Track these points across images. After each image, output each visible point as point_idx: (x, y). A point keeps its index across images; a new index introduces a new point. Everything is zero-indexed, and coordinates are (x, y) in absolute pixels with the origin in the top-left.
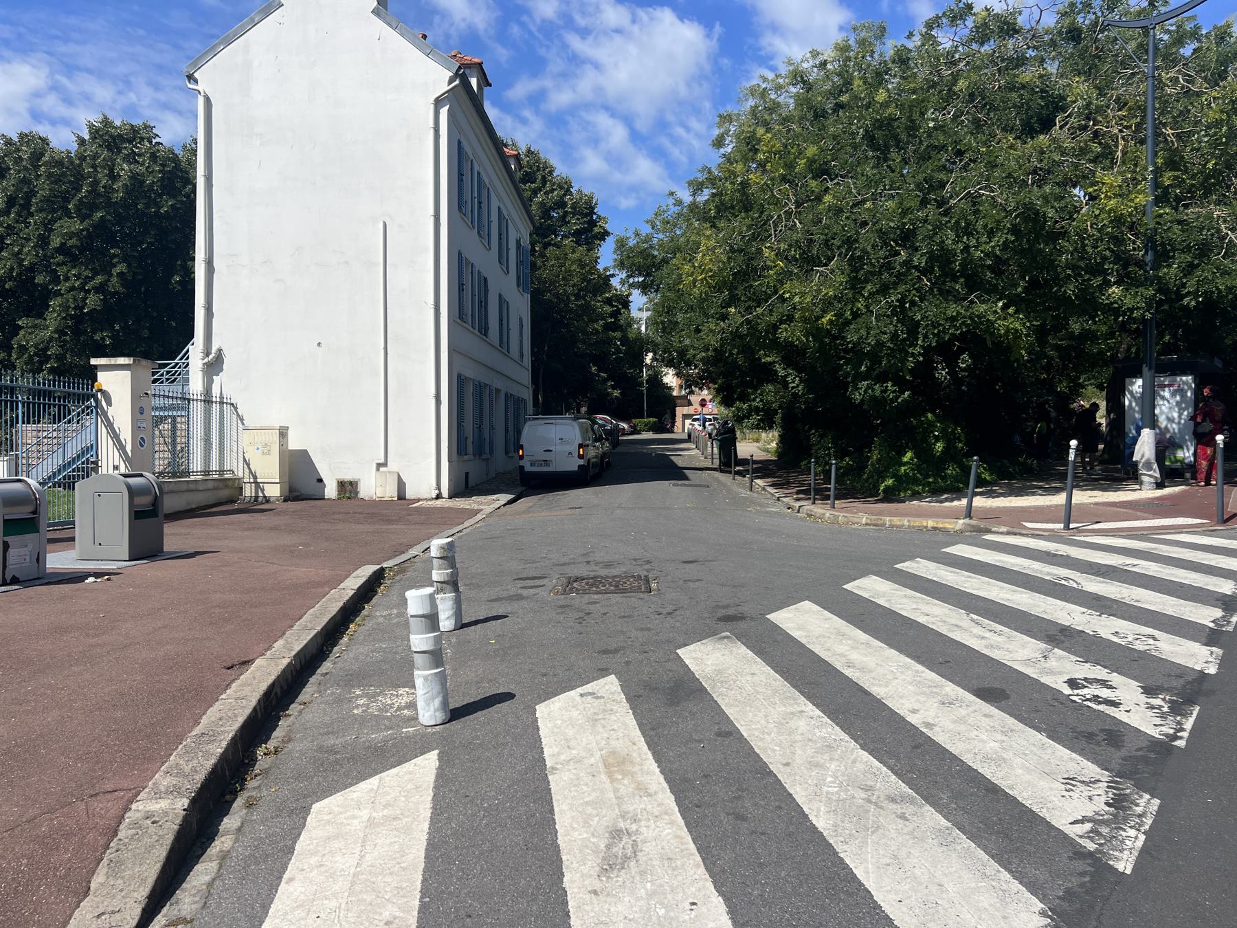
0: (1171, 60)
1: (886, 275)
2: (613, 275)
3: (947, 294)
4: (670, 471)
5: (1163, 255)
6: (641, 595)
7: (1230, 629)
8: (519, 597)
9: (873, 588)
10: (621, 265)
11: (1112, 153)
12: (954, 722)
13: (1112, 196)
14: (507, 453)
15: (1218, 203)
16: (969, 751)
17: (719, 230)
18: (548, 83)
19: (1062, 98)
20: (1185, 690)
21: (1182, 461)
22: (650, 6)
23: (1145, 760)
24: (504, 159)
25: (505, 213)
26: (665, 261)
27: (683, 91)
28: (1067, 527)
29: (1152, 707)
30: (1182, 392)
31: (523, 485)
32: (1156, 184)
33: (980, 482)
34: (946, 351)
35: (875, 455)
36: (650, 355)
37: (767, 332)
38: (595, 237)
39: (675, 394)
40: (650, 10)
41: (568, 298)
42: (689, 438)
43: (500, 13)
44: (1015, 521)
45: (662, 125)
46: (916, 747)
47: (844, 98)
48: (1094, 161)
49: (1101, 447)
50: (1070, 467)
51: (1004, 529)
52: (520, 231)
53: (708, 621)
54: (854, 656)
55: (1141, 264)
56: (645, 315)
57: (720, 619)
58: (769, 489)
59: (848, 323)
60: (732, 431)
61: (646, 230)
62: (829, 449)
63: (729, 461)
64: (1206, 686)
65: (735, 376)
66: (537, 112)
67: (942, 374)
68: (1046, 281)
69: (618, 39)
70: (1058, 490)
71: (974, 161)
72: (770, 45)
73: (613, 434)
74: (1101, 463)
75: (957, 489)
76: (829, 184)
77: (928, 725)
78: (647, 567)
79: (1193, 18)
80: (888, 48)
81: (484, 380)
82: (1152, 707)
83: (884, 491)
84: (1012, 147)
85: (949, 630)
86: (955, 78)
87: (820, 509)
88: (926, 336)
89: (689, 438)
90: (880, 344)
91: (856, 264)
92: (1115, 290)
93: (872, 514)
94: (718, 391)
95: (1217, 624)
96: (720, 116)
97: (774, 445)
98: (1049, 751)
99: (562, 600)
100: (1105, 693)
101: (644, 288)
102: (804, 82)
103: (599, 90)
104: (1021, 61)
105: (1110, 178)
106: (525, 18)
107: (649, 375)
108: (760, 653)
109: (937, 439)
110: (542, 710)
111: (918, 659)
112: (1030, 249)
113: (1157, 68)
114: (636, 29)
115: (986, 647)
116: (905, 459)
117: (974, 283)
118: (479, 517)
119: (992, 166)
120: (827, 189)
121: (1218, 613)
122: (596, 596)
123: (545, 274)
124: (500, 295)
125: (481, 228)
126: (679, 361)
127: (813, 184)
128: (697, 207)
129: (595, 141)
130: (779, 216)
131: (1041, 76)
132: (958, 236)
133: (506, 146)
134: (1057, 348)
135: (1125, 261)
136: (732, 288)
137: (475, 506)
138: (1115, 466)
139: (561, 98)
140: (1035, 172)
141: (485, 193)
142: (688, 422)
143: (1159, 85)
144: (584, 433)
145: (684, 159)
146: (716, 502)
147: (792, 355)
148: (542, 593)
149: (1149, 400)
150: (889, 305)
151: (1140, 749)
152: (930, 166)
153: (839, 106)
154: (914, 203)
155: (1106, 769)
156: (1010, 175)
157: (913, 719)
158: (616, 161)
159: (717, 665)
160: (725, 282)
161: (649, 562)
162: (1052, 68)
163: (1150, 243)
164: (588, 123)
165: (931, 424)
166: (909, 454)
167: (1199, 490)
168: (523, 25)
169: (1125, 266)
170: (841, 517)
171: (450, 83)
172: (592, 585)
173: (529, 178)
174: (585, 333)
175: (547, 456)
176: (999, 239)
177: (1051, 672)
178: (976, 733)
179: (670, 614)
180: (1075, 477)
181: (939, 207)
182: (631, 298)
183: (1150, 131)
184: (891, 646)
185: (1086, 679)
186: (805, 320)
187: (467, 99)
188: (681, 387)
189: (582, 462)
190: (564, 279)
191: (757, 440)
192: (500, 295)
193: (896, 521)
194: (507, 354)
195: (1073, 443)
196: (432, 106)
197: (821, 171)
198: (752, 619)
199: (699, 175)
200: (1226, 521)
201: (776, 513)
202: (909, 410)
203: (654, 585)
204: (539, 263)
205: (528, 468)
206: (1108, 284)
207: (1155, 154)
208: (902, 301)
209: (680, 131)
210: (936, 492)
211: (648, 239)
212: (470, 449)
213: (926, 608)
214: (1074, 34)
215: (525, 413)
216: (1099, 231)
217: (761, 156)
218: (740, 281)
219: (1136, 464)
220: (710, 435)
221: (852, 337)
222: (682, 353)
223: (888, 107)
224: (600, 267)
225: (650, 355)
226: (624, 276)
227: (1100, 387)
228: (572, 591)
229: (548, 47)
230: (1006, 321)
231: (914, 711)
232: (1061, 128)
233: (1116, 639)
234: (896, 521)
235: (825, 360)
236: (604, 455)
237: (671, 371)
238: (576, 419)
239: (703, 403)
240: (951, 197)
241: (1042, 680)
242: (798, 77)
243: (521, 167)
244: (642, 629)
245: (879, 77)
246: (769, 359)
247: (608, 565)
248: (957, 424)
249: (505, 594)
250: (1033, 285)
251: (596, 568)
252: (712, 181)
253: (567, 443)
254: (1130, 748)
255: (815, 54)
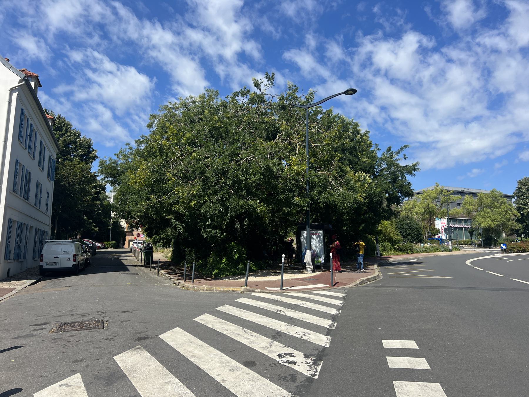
0: (314, 121)
1: (216, 187)
2: (98, 176)
3: (239, 196)
4: (121, 267)
5: (312, 187)
6: (99, 330)
7: (334, 328)
8: (31, 335)
9: (206, 319)
10: (102, 172)
11: (296, 150)
12: (234, 378)
13: (294, 166)
14: (33, 258)
15: (328, 171)
16: (239, 391)
17: (148, 162)
18: (75, 88)
19: (279, 129)
20: (317, 355)
21: (320, 262)
22: (125, 65)
23: (303, 386)
24: (46, 120)
25: (44, 143)
26: (123, 172)
27: (138, 101)
28: (282, 289)
29: (307, 363)
30: (319, 236)
31: (41, 274)
32: (309, 163)
33: (251, 271)
34: (240, 218)
35: (211, 259)
36: (114, 213)
37: (168, 206)
38: (91, 158)
39: (126, 230)
40: (125, 67)
41: (74, 185)
42: (131, 251)
43: (53, 55)
44: (262, 287)
45: (128, 114)
46: (218, 392)
47: (202, 117)
48: (290, 152)
49: (294, 256)
50: (282, 265)
51: (259, 290)
52: (51, 152)
53: (131, 341)
54: (196, 352)
55: (305, 189)
56: (113, 194)
57: (136, 340)
58: (167, 275)
59: (201, 205)
60: (151, 248)
61: (115, 158)
62: (193, 256)
63: (149, 262)
64: (326, 352)
65: (154, 224)
66: (68, 100)
67: (238, 226)
68: (275, 193)
69: (110, 76)
70: (279, 274)
71: (250, 147)
72: (176, 89)
73: (93, 250)
74: (295, 262)
75: (242, 274)
76: (195, 149)
77: (224, 381)
78: (103, 315)
79: (320, 107)
80: (218, 101)
81: (23, 221)
82: (307, 363)
83: (215, 275)
84: (262, 143)
85: (235, 337)
86: (243, 116)
87: (188, 284)
88: (231, 212)
89: (131, 251)
90: (214, 214)
91: (205, 181)
92: (297, 198)
93: (209, 285)
94: (146, 230)
95: (330, 327)
96: (151, 115)
97: (170, 254)
98: (270, 387)
99: (55, 335)
100: (291, 359)
101: (113, 183)
102: (186, 108)
103: (100, 95)
104: (265, 113)
105: (295, 159)
106: (66, 59)
107: (113, 222)
108: (154, 354)
109: (235, 253)
110: (79, 374)
111: (222, 351)
112: (268, 182)
113: (309, 123)
114: (119, 73)
115: (249, 343)
116: (223, 261)
117: (249, 193)
118: (14, 292)
119: (255, 150)
120: (194, 151)
121: (330, 322)
122: (74, 332)
123: (63, 173)
124: (38, 181)
125: (30, 150)
126: (127, 216)
127: (188, 148)
128: (139, 151)
129: (96, 116)
130: (174, 159)
131: (272, 120)
132: (243, 174)
133: (48, 113)
134: (278, 218)
135: (300, 188)
136: (152, 186)
137: (12, 287)
138: (298, 266)
139: (81, 96)
140: (270, 154)
141: (34, 134)
142: (131, 243)
143: (310, 128)
144: (77, 249)
145: (137, 129)
146: (142, 281)
147: (179, 217)
148: (45, 332)
149: (309, 239)
150: (218, 199)
151: (302, 382)
152: (234, 147)
153: (200, 120)
154: (227, 161)
155: (290, 392)
156: (261, 154)
157: (218, 379)
158: (105, 125)
159: (132, 363)
160: (149, 184)
161: (105, 313)
162: (276, 117)
163: (308, 183)
164: (93, 108)
165: (233, 247)
166: (225, 259)
167: (328, 273)
168: (64, 62)
169: (301, 190)
170: (196, 287)
171: (19, 82)
172: (73, 327)
173: (58, 129)
174: (82, 201)
175: (56, 260)
176: (258, 177)
177: (273, 352)
178: (242, 382)
179: (112, 338)
180: (285, 268)
181: (236, 163)
182: (106, 187)
183: (307, 144)
184: (211, 346)
185: (285, 354)
186: (184, 203)
187: (28, 91)
188: (128, 228)
189: (75, 263)
190: (72, 176)
191: (163, 252)
192: (38, 181)
193: (218, 288)
194: (39, 209)
195: (283, 256)
196: (9, 92)
197: (192, 143)
198: (152, 338)
199: (141, 138)
200: (334, 285)
201: (168, 286)
202: (226, 241)
203: (106, 325)
204: (60, 167)
205: (45, 266)
206: (294, 196)
207: (309, 152)
208: (222, 198)
209: (136, 117)
210: (235, 275)
211: (115, 162)
212: (12, 256)
213: (227, 327)
214: (284, 107)
215: (46, 238)
216: (292, 177)
217: (168, 134)
218: (156, 184)
219: (305, 263)
220: (141, 249)
221: (202, 211)
222: (129, 213)
223: (218, 122)
224: (92, 172)
225: (114, 213)
226: (103, 177)
227: (294, 233)
228: (61, 330)
229: (76, 73)
230: (262, 208)
231: (218, 375)
232: (279, 139)
233: (296, 336)
234: (218, 288)
235: (193, 219)
236: (87, 259)
237: (124, 221)
238: (73, 242)
239: (138, 235)
240: (241, 159)
241: (269, 356)
242: (184, 105)
243: (55, 124)
244: (97, 348)
245: (217, 111)
246: (169, 217)
247: (83, 315)
248: (243, 247)
249: (23, 334)
250: (270, 194)
251: (76, 317)
252: (147, 141)
253: (67, 253)
254: (299, 381)
255: (191, 97)
